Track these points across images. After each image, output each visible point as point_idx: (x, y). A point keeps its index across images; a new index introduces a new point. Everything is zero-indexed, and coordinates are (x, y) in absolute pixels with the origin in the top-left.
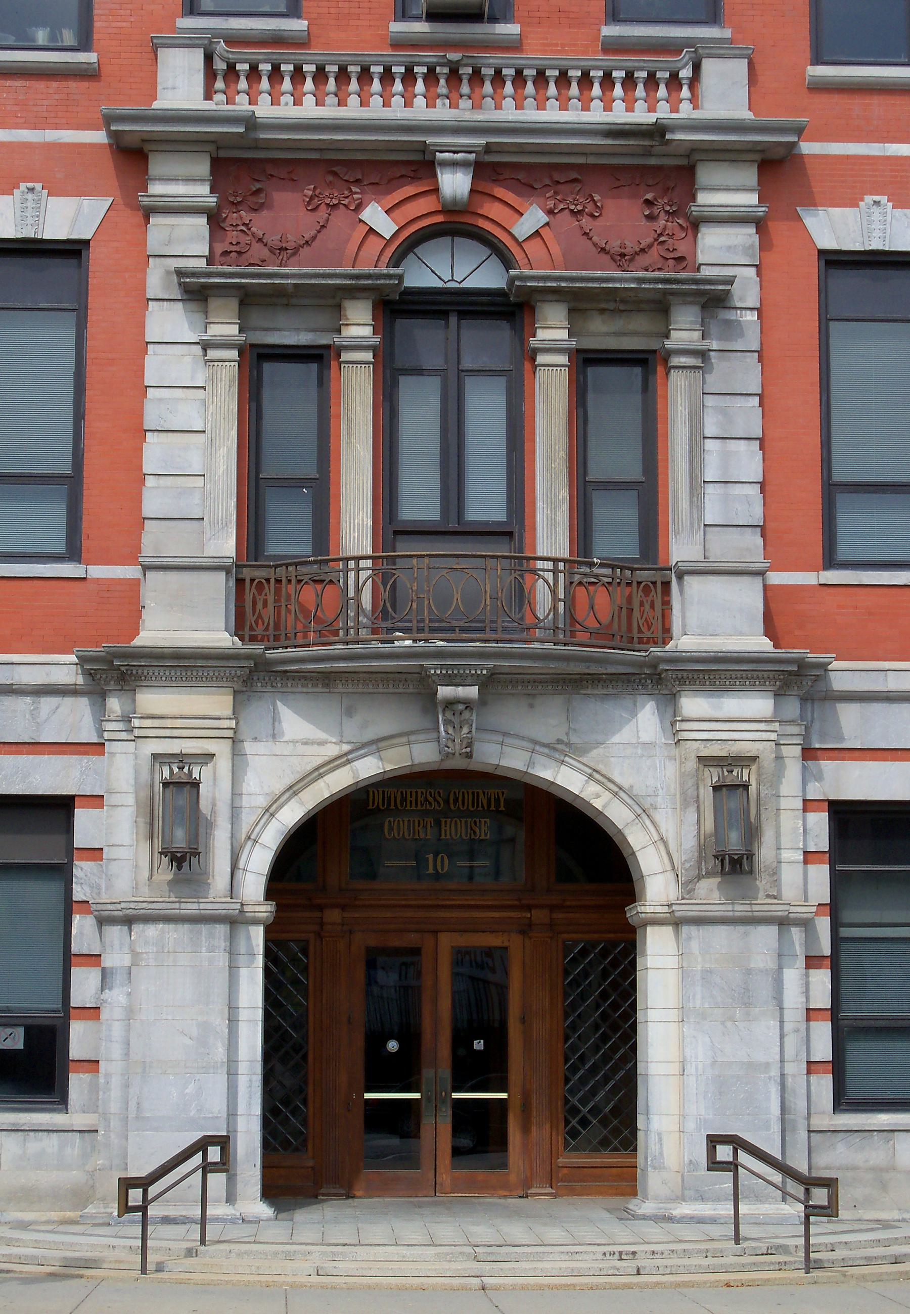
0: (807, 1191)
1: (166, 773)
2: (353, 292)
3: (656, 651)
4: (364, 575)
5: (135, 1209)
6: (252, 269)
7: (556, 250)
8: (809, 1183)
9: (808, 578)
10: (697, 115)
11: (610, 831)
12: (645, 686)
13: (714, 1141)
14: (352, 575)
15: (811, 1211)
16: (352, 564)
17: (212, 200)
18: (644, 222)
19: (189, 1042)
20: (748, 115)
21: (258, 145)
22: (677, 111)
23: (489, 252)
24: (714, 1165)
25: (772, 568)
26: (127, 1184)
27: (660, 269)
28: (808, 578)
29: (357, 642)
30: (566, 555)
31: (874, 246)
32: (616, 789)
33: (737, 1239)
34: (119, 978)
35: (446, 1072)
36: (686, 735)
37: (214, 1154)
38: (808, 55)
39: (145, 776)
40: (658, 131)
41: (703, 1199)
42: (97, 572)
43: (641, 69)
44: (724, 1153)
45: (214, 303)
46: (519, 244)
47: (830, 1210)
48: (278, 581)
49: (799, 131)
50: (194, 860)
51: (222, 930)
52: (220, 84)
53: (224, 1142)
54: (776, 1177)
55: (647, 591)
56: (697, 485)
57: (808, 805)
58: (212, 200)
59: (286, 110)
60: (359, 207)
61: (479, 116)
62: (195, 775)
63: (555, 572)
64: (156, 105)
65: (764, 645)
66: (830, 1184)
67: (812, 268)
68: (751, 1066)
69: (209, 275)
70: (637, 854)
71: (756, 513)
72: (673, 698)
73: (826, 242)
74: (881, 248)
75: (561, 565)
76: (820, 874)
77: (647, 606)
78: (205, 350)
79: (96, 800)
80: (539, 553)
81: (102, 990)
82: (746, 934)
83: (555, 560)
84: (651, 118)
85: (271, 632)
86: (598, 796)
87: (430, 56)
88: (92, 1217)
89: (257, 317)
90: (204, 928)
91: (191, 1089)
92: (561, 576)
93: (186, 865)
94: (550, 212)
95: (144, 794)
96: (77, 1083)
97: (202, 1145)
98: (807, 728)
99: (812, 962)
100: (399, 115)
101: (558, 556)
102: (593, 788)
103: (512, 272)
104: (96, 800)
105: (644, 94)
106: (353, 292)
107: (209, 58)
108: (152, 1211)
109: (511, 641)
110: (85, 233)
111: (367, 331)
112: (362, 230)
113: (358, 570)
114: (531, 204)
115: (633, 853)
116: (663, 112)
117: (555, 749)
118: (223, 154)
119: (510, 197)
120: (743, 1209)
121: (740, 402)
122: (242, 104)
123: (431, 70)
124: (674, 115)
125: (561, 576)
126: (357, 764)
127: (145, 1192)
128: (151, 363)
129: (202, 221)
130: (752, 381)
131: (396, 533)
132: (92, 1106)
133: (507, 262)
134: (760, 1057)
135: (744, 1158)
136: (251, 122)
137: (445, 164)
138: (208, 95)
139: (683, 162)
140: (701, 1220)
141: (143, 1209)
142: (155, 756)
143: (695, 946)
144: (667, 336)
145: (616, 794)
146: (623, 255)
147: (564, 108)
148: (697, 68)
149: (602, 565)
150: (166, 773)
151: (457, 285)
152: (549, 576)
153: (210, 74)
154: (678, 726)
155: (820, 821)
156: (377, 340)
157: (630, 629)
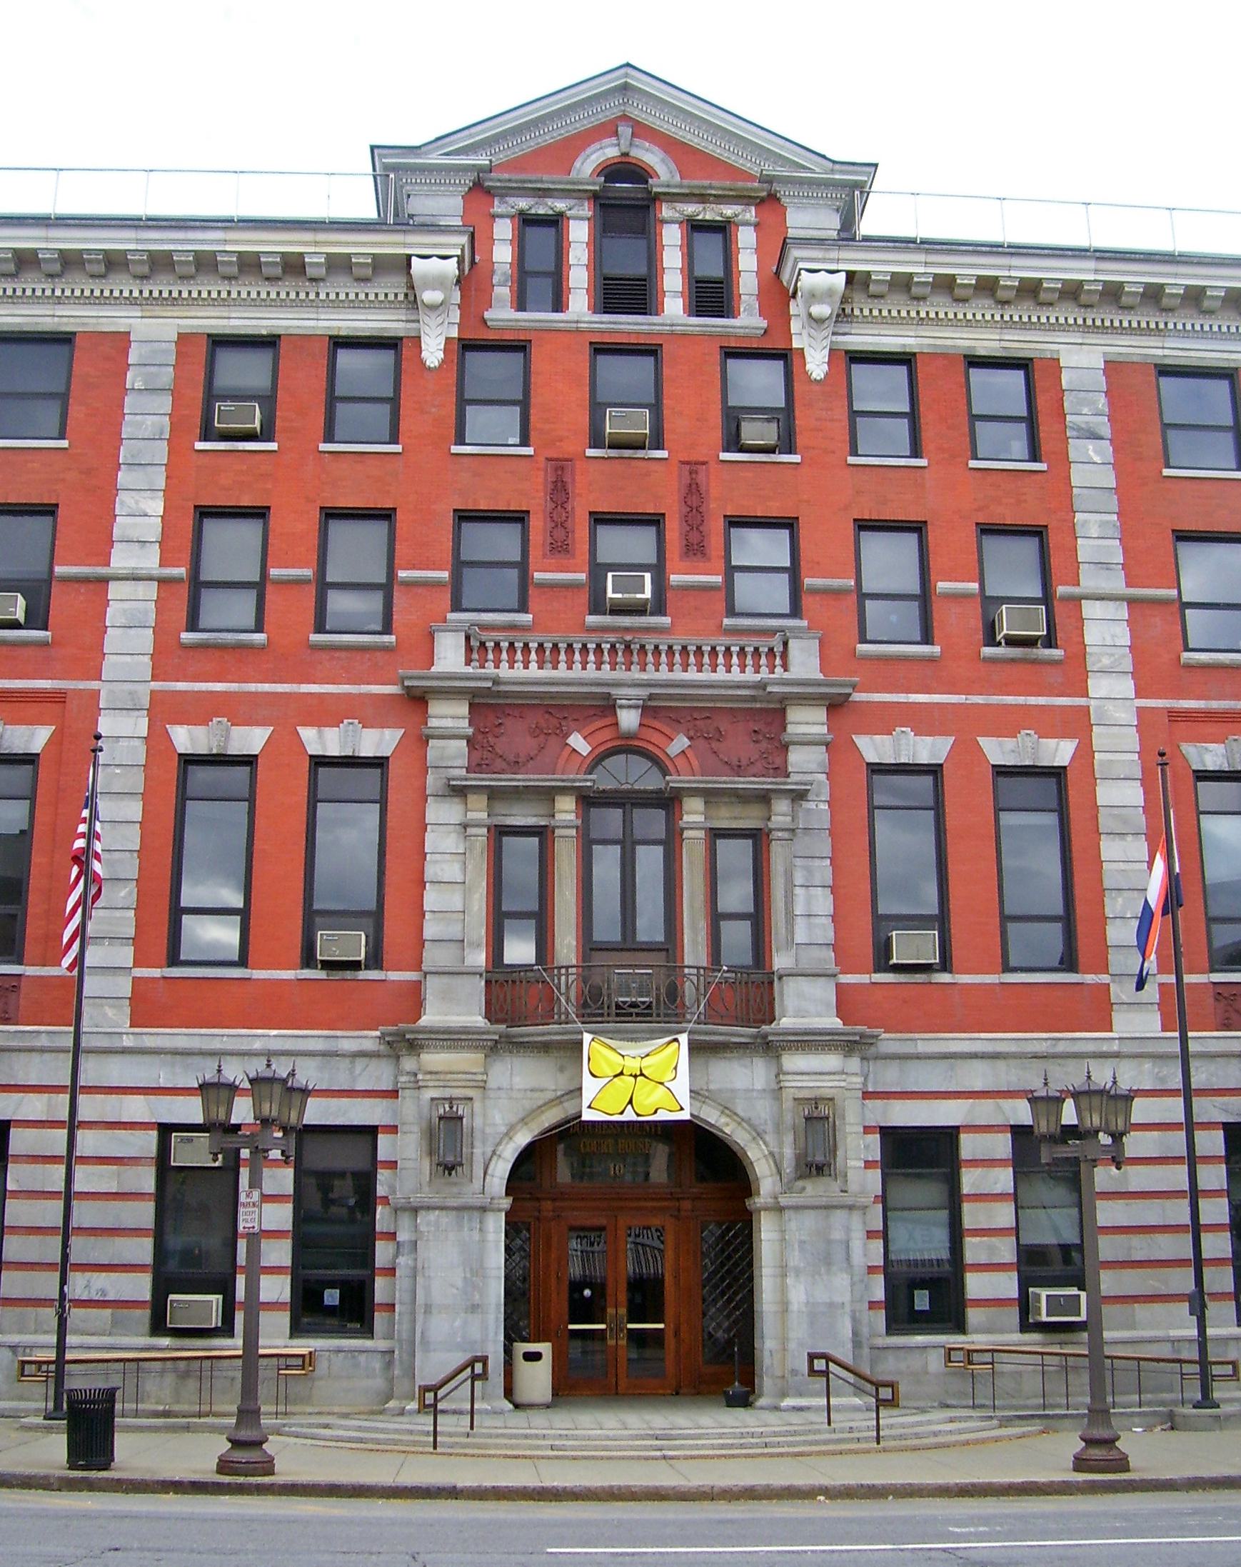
0: (877, 1390)
1: (441, 1111)
2: (563, 790)
3: (765, 1028)
4: (571, 978)
5: (430, 1406)
6: (494, 776)
7: (695, 763)
8: (878, 1385)
9: (864, 978)
10: (786, 675)
11: (735, 1148)
12: (757, 1052)
13: (812, 1357)
14: (563, 978)
15: (881, 1403)
16: (563, 971)
17: (470, 731)
18: (752, 745)
19: (455, 1291)
20: (821, 676)
21: (499, 694)
22: (773, 673)
23: (650, 764)
24: (812, 1372)
25: (843, 972)
26: (426, 1389)
27: (763, 776)
28: (864, 978)
29: (567, 1023)
30: (705, 965)
31: (902, 761)
32: (739, 1120)
33: (829, 1423)
34: (406, 1249)
35: (623, 1311)
36: (787, 1084)
37: (478, 1368)
38: (980, 636)
39: (426, 1110)
40: (762, 685)
41: (801, 1395)
42: (394, 976)
43: (749, 646)
44: (820, 1364)
45: (472, 798)
46: (671, 759)
47: (892, 1403)
48: (514, 982)
49: (854, 687)
50: (459, 1169)
51: (476, 1214)
52: (475, 656)
53: (484, 1360)
54: (851, 1378)
55: (502, 986)
56: (790, 917)
57: (867, 1130)
58: (470, 731)
59: (519, 672)
60: (567, 735)
61: (644, 676)
62: (460, 1112)
63: (698, 975)
64: (433, 669)
65: (837, 1023)
66: (891, 1385)
67: (863, 773)
68: (831, 1305)
69: (466, 780)
70: (755, 1164)
71: (830, 936)
72: (778, 1057)
73: (871, 757)
74: (907, 761)
75: (702, 971)
76: (875, 1176)
77: (502, 996)
78: (465, 828)
79: (393, 1129)
80: (686, 963)
81: (397, 1257)
82: (828, 1217)
83: (698, 968)
84: (758, 677)
85: (563, 1017)
86: (727, 1125)
87: (612, 638)
88: (393, 1409)
89: (500, 807)
90: (466, 1215)
91: (457, 1323)
92: (702, 978)
93: (453, 1172)
94: (690, 738)
95: (424, 1125)
96: (379, 1318)
97: (471, 1364)
98: (865, 1079)
99: (870, 1234)
100: (722, 678)
101: (700, 965)
102: (724, 1120)
103: (667, 778)
104: (393, 1129)
105: (623, 660)
106: (563, 790)
107: (468, 638)
108: (440, 1406)
109: (669, 1022)
110: (386, 752)
111: (572, 817)
112: (568, 750)
113: (567, 975)
114: (679, 733)
115: (752, 1163)
116: (764, 674)
117: (698, 1094)
118: (477, 701)
119: (667, 730)
120: (832, 1401)
121: (817, 862)
122: (490, 669)
123: (613, 646)
124: (772, 676)
125: (702, 978)
126: (566, 1104)
127: (436, 1395)
128: (429, 837)
129: (464, 743)
130: (825, 847)
131: (592, 949)
132: (389, 1336)
133: (665, 772)
134: (838, 1299)
135: (832, 1366)
136: (496, 681)
137: (622, 707)
138: (468, 662)
139: (778, 706)
140: (800, 1409)
141: (435, 1406)
142: (432, 1099)
143: (793, 1225)
144: (769, 819)
145: (739, 1124)
146: (739, 766)
147: (643, 669)
148: (785, 644)
149: (728, 971)
150: (441, 1111)
151: (630, 787)
152: (695, 979)
153: (469, 649)
154: (781, 1077)
155: (875, 1139)
156: (579, 822)
157: (748, 1014)
